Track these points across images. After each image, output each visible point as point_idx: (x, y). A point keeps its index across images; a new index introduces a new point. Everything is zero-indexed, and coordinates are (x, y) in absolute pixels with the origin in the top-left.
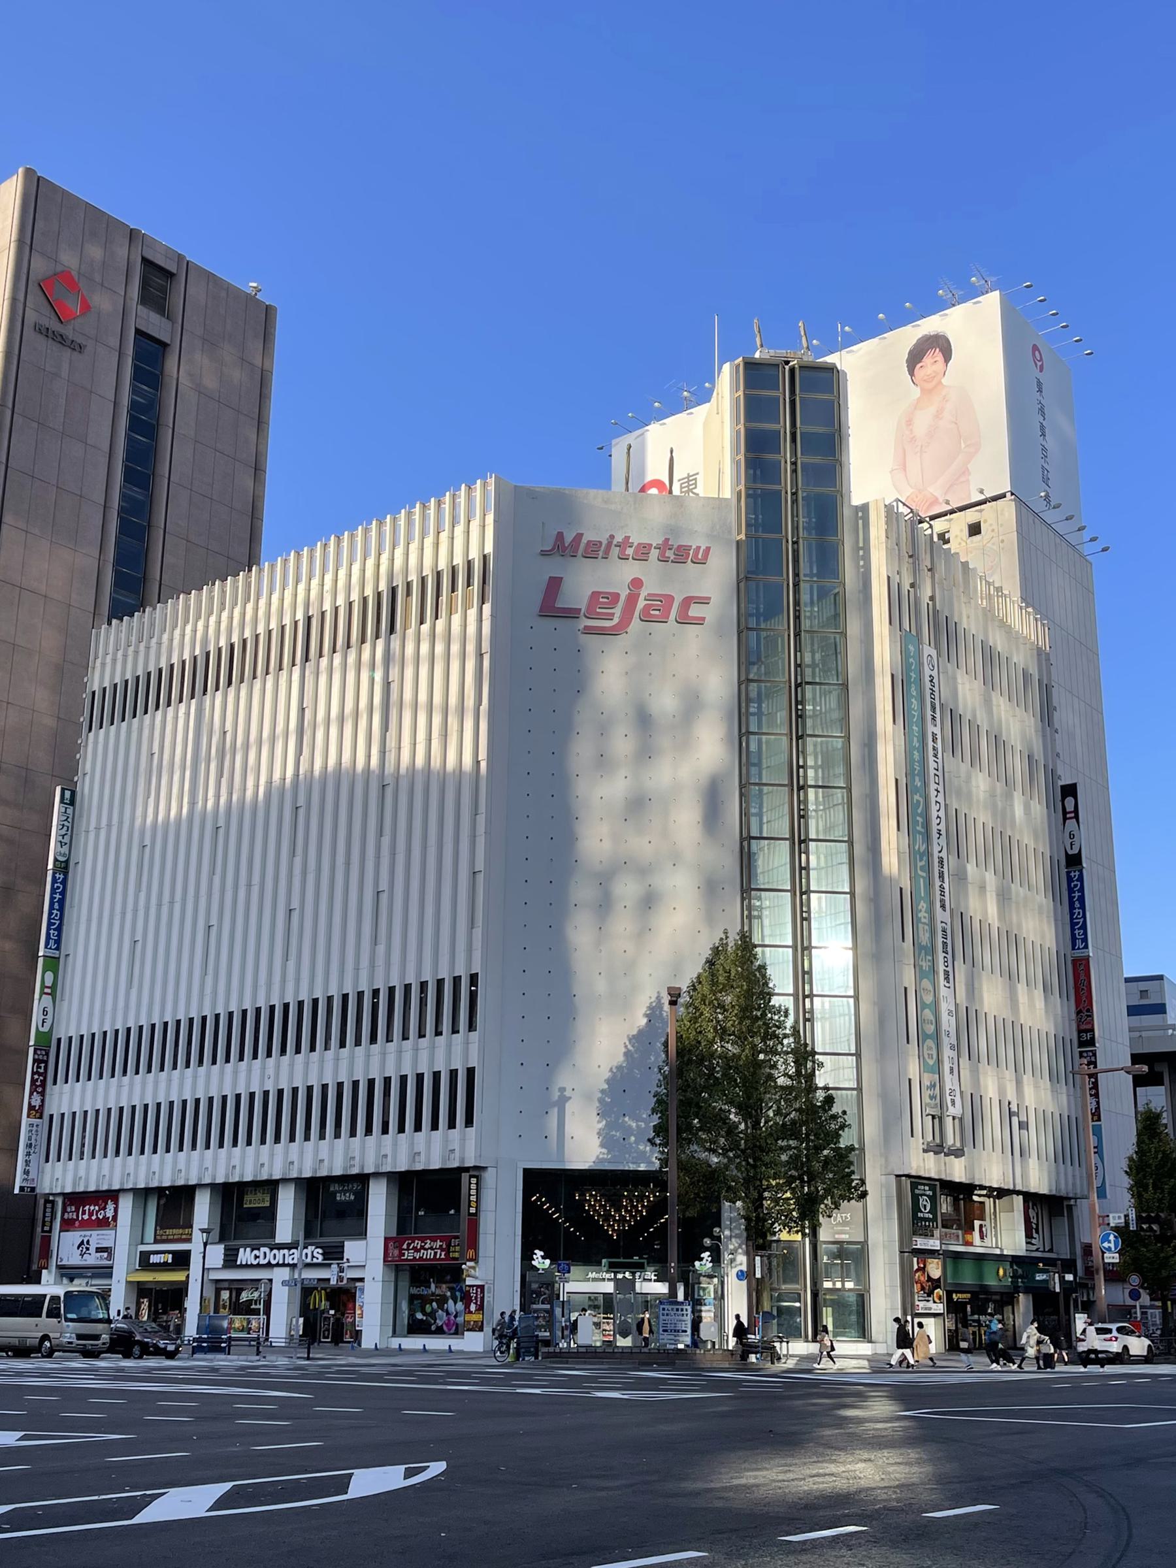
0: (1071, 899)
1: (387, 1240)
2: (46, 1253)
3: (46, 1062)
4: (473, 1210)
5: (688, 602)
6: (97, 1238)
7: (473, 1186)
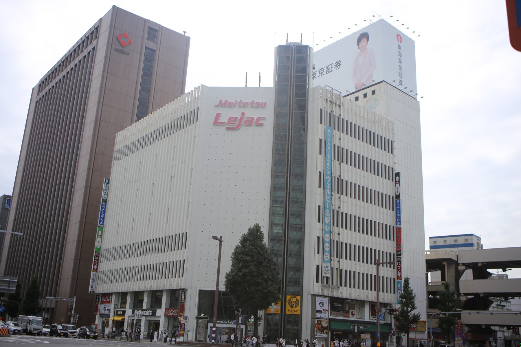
0: (396, 209)
1: (166, 309)
2: (96, 309)
3: (99, 257)
4: (183, 301)
5: (258, 119)
6: (108, 306)
7: (183, 294)
